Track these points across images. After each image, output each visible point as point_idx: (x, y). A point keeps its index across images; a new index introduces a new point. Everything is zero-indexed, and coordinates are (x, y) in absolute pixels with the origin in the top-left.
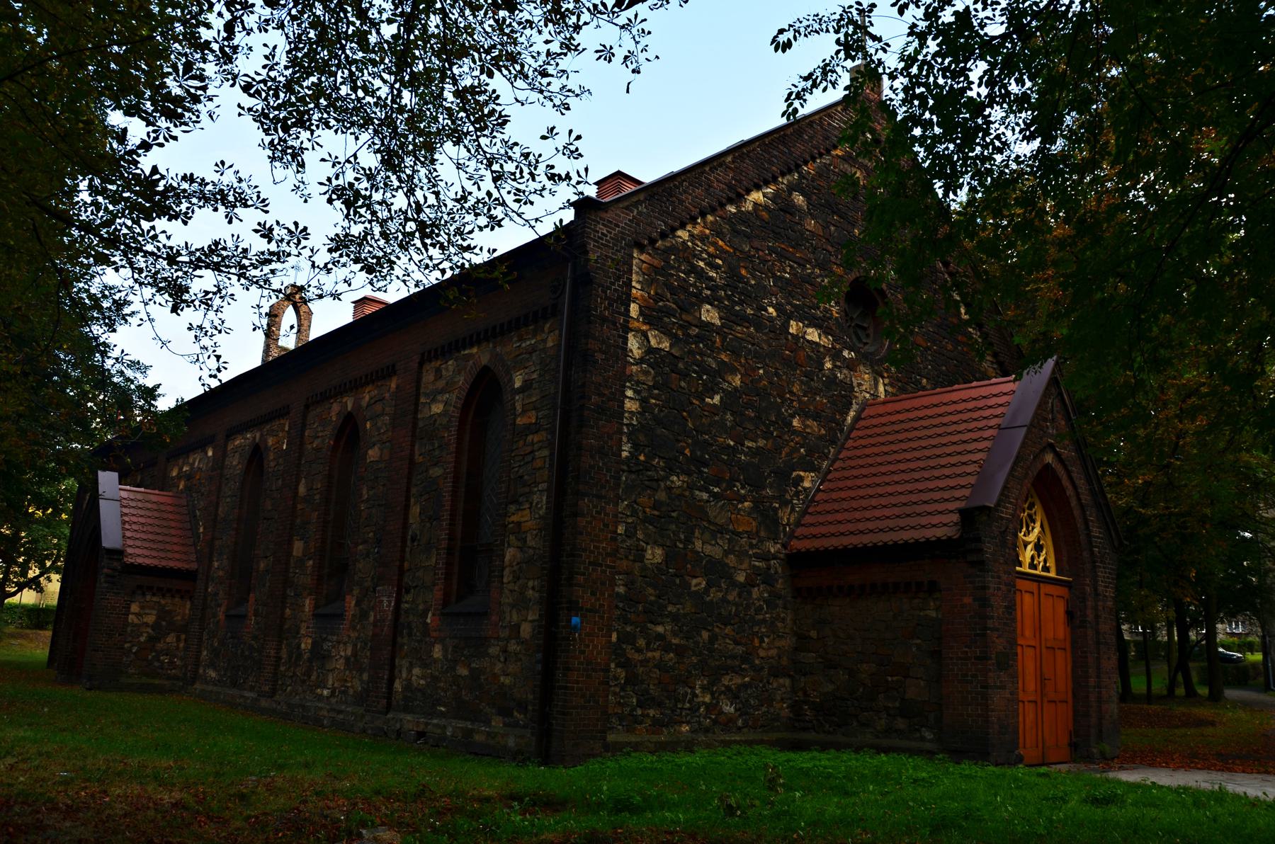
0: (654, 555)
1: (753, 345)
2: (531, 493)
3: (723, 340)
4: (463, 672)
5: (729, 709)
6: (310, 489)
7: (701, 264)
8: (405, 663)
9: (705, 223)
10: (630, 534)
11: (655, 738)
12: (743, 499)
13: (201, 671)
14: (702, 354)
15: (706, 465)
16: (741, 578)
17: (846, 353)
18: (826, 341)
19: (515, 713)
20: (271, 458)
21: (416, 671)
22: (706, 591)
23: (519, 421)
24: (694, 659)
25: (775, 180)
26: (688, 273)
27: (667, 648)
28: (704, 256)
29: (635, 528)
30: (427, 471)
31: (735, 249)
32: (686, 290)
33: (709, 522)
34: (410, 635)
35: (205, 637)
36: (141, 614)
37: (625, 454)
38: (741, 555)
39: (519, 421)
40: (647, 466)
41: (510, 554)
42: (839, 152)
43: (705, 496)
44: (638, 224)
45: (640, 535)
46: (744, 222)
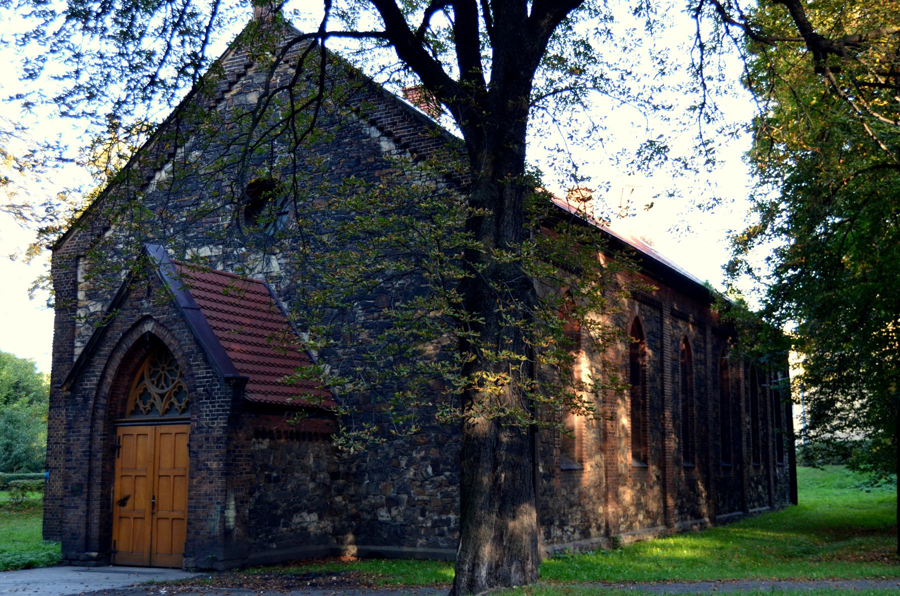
46: (151, 201)
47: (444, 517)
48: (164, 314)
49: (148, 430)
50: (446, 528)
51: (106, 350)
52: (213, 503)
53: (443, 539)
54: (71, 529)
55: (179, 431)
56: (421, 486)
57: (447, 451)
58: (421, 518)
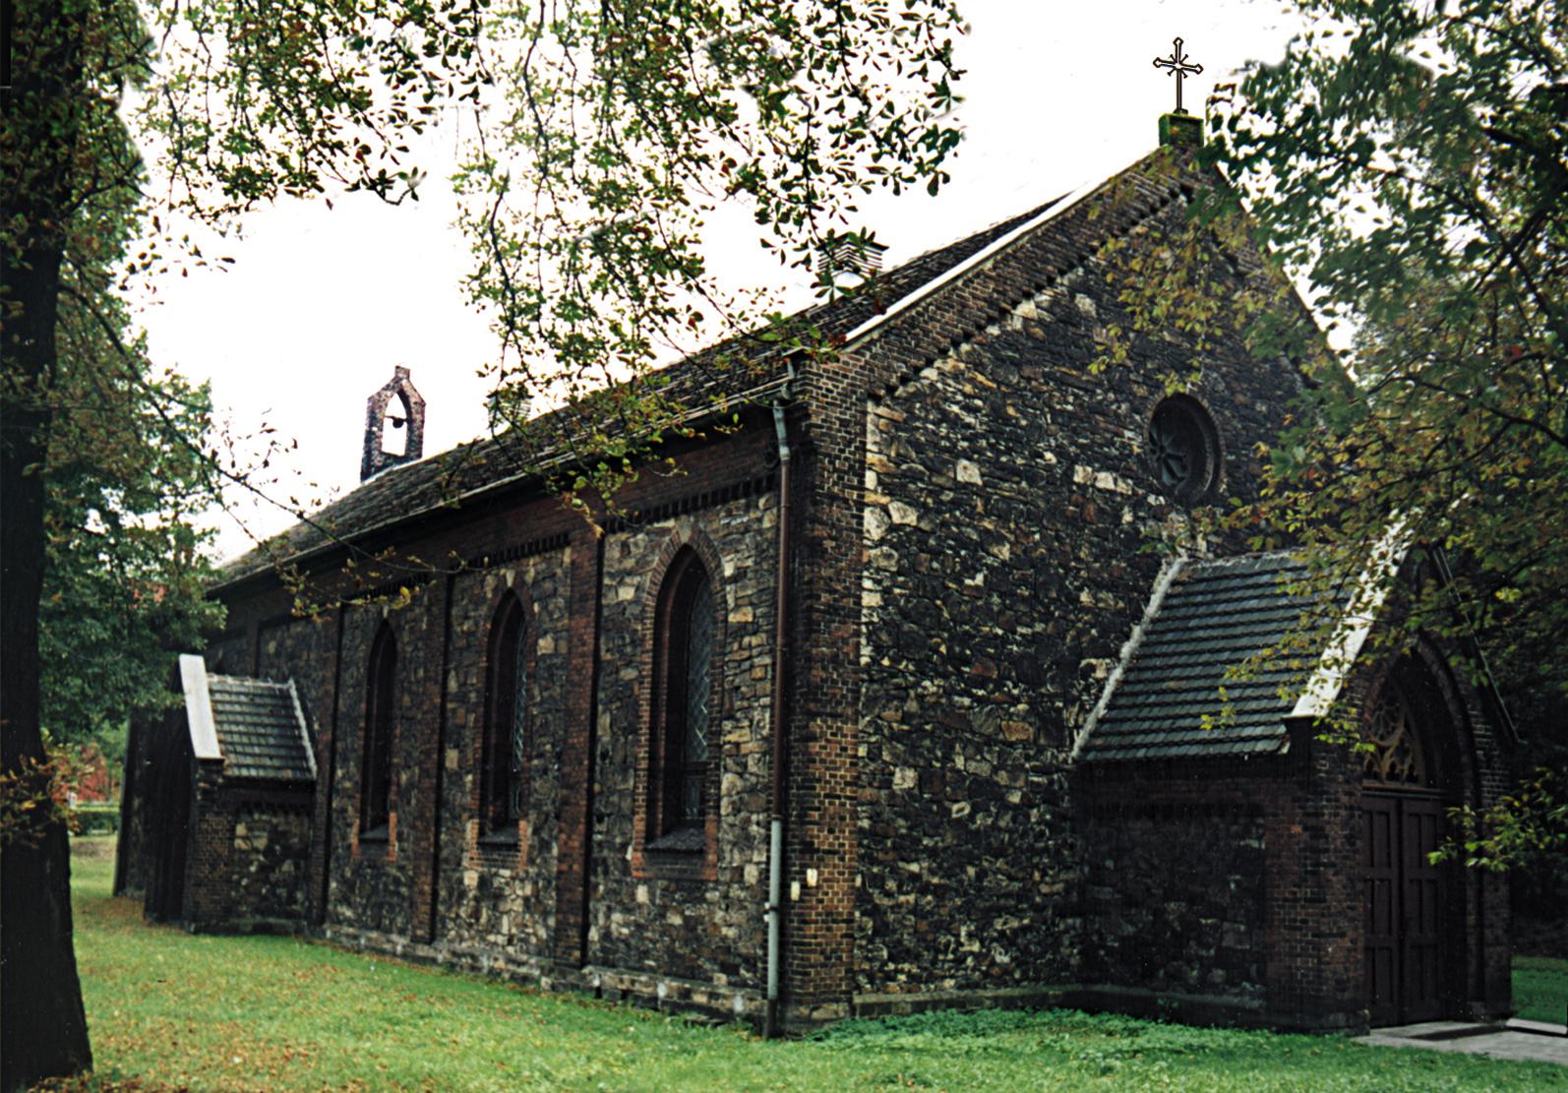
0: (905, 779)
1: (1025, 503)
2: (750, 707)
3: (987, 501)
4: (677, 920)
5: (1002, 958)
6: (462, 685)
7: (955, 409)
8: (602, 908)
9: (958, 354)
10: (874, 755)
11: (909, 998)
12: (1016, 700)
13: (330, 907)
14: (958, 524)
15: (967, 663)
16: (1015, 798)
17: (1151, 499)
18: (1123, 487)
19: (742, 972)
20: (406, 639)
21: (617, 917)
22: (972, 817)
23: (732, 618)
24: (958, 901)
25: (1051, 282)
26: (937, 423)
27: (924, 890)
28: (959, 398)
29: (880, 750)
30: (617, 671)
31: (999, 383)
32: (936, 445)
33: (974, 733)
34: (606, 873)
35: (332, 865)
36: (249, 837)
37: (864, 660)
38: (1016, 770)
39: (732, 618)
40: (893, 673)
41: (727, 780)
42: (1139, 229)
43: (967, 701)
44: (871, 370)
45: (886, 757)
46: (1010, 346)
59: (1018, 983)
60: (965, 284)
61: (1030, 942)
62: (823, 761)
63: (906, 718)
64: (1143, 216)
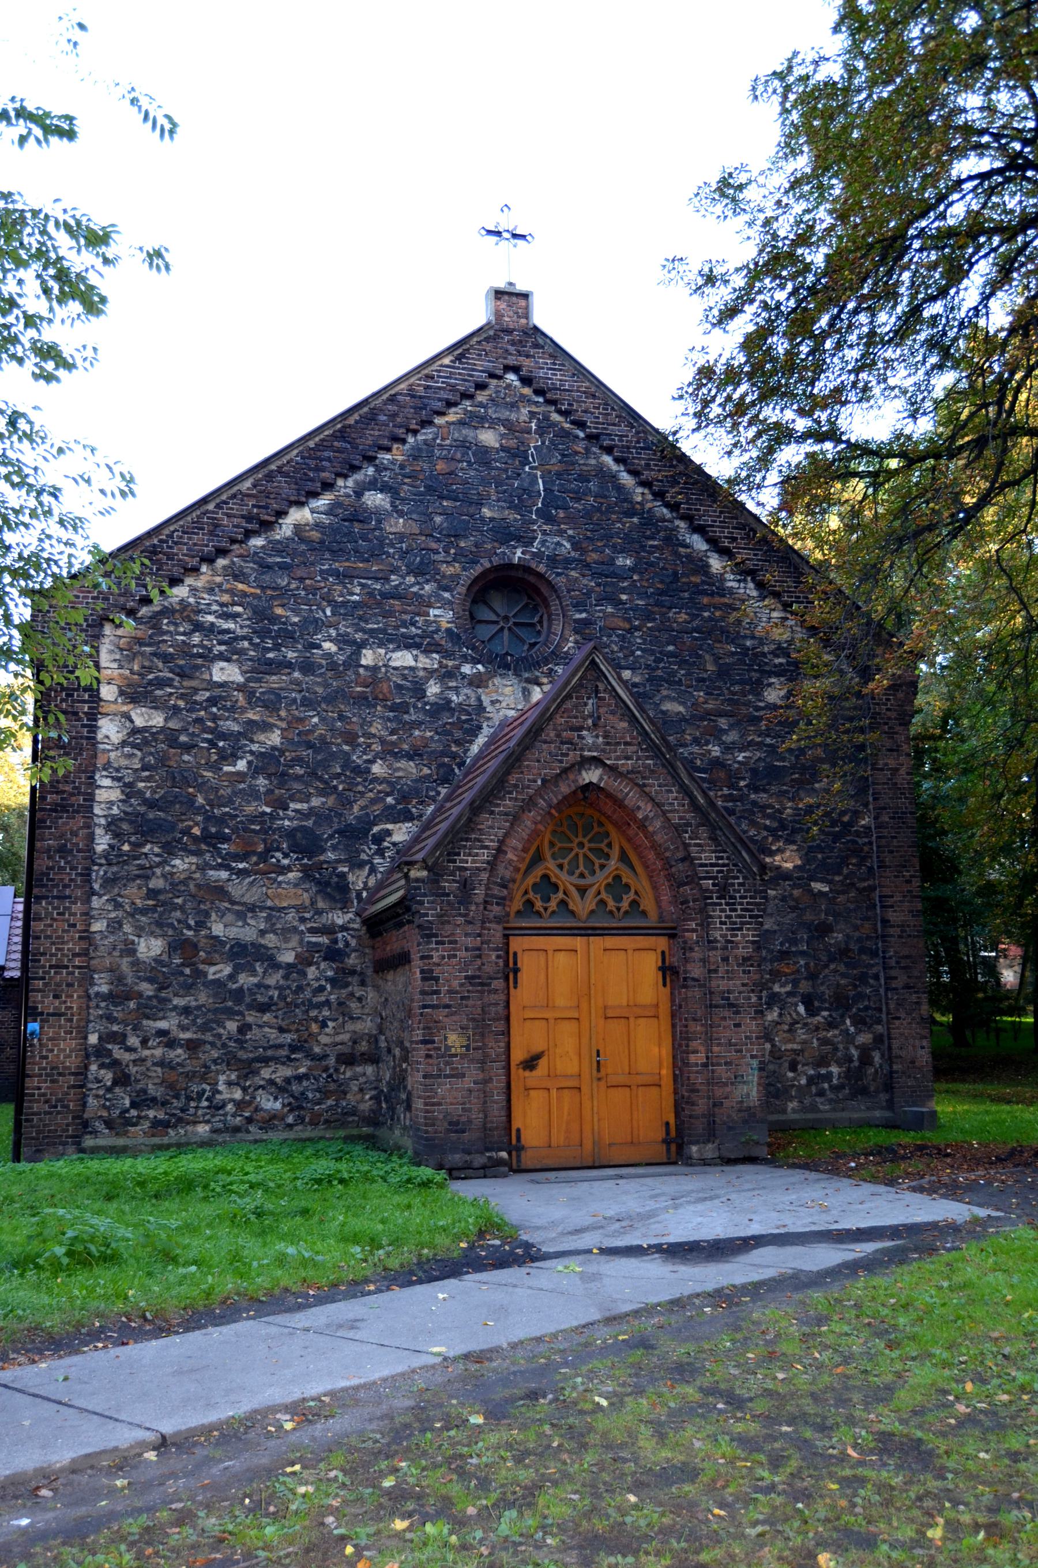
7: (211, 618)
22: (232, 977)
25: (328, 486)
28: (215, 607)
43: (224, 875)
46: (280, 552)
47: (823, 1071)
48: (627, 758)
49: (578, 942)
50: (826, 1086)
51: (507, 804)
52: (744, 1057)
53: (822, 1099)
54: (447, 1114)
55: (639, 946)
56: (790, 1031)
57: (822, 984)
58: (790, 1075)
59: (290, 1126)
60: (218, 506)
61: (307, 1089)
62: (47, 937)
63: (152, 894)
64: (450, 404)
